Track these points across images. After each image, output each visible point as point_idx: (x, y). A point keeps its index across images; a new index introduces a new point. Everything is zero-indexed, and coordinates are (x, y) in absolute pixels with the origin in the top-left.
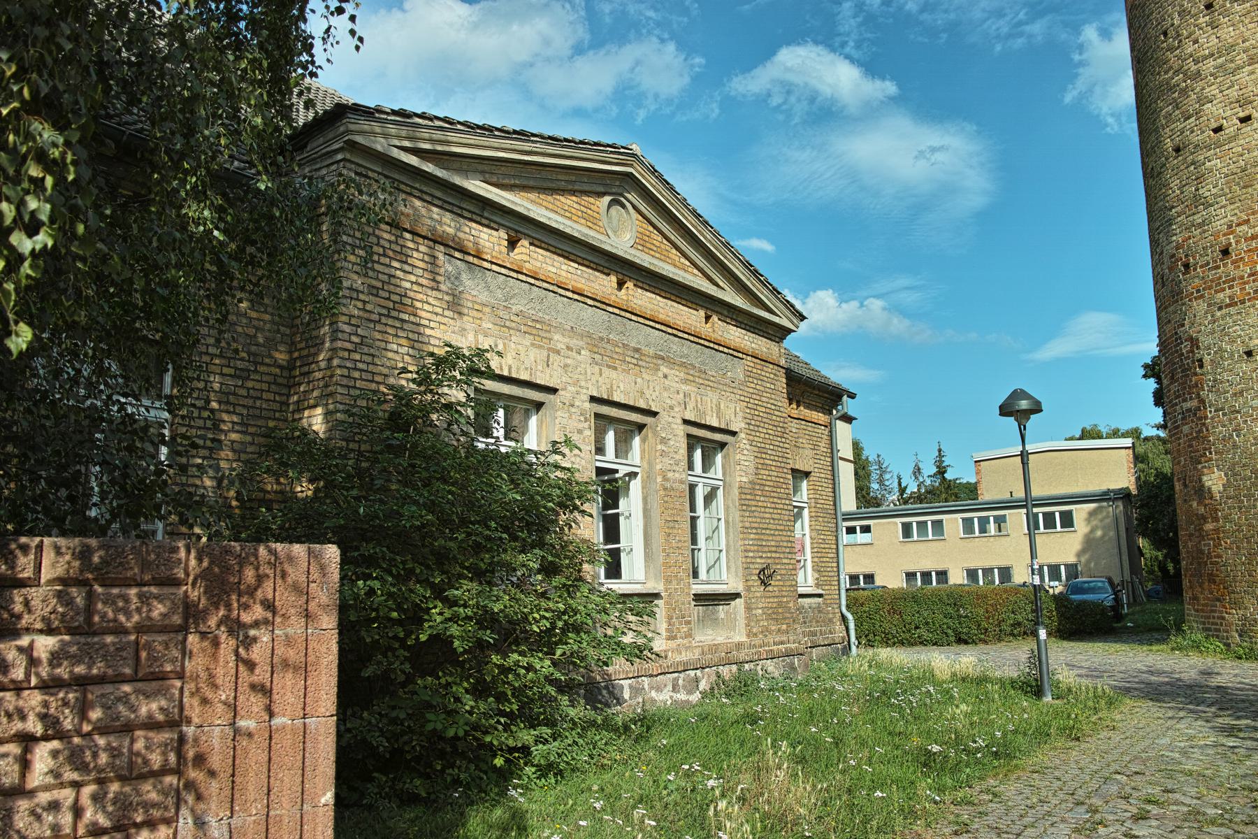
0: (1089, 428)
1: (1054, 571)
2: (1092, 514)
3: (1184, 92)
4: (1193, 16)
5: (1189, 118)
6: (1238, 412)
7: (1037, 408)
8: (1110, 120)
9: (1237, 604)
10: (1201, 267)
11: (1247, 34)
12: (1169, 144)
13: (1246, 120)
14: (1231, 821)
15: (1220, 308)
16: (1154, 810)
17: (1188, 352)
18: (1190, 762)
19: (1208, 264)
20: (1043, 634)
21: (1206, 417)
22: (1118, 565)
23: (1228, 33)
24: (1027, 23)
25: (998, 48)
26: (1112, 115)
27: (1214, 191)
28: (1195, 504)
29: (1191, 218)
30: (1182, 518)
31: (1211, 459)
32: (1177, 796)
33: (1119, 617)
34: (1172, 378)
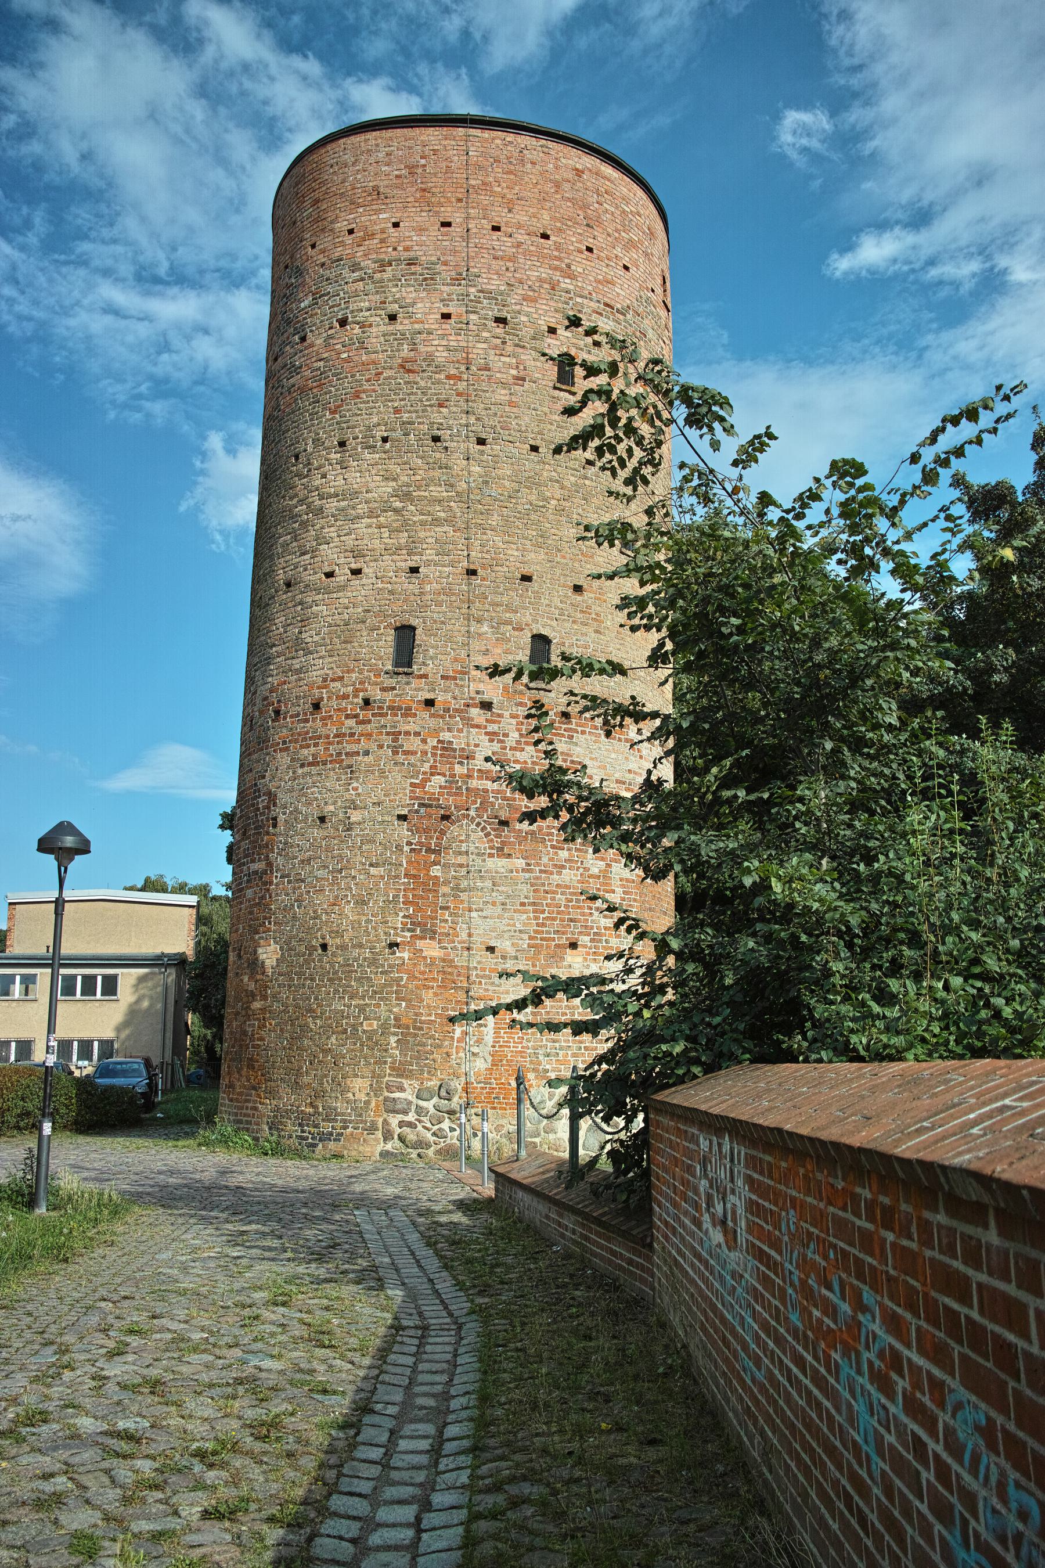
0: (153, 878)
1: (85, 1047)
2: (142, 979)
3: (304, 524)
4: (325, 449)
5: (304, 554)
6: (303, 881)
7: (84, 848)
8: (218, 537)
9: (272, 1093)
10: (291, 717)
11: (372, 485)
12: (281, 576)
13: (356, 572)
14: (214, 1345)
15: (302, 766)
16: (134, 1341)
17: (264, 808)
18: (188, 1279)
19: (298, 715)
20: (47, 1128)
21: (271, 883)
22: (160, 1044)
23: (355, 479)
24: (147, 400)
25: (112, 415)
26: (221, 532)
27: (316, 638)
28: (246, 979)
29: (289, 662)
30: (231, 993)
31: (269, 930)
32: (164, 1321)
33: (150, 1105)
34: (244, 834)
